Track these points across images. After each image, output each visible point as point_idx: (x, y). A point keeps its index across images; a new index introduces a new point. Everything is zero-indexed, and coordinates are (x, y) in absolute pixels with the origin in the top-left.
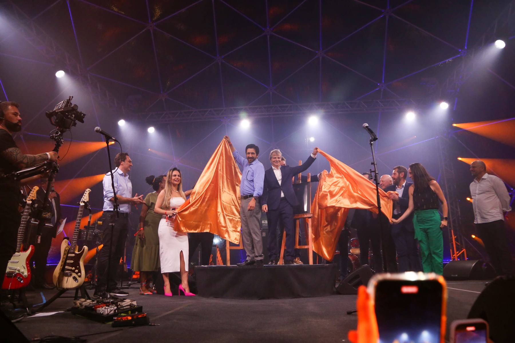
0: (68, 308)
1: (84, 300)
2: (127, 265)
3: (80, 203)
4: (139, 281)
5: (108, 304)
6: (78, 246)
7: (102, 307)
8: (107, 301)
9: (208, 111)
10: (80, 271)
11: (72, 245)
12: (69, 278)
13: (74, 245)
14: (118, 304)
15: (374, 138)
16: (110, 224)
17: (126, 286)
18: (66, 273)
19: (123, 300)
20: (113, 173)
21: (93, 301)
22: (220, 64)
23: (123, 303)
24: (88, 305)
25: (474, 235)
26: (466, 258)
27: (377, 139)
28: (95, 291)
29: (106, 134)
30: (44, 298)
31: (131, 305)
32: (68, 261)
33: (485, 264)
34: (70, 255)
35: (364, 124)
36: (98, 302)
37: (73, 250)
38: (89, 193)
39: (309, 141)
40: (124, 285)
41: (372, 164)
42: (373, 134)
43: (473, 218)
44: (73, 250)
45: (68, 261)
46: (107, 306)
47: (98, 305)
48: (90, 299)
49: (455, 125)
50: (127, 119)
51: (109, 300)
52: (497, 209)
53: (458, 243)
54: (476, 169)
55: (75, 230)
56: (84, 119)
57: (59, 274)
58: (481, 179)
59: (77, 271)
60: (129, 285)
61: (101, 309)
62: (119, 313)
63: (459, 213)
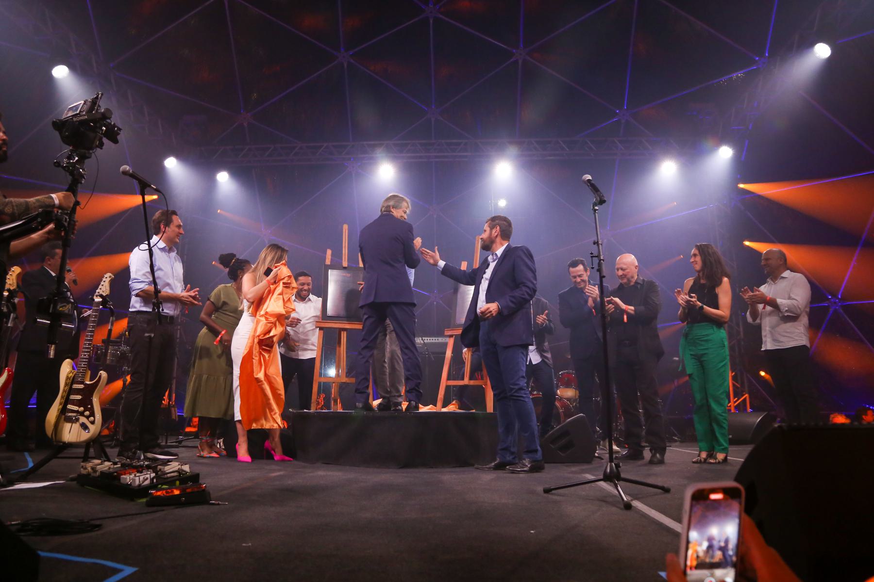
0: (71, 476)
1: (99, 461)
2: (176, 409)
3: (95, 297)
4: (196, 435)
5: (141, 470)
6: (89, 372)
7: (130, 474)
8: (138, 464)
9: (324, 147)
10: (92, 414)
11: (80, 370)
12: (74, 425)
13: (83, 370)
14: (158, 470)
15: (601, 199)
16: (147, 335)
17: (174, 444)
18: (69, 416)
19: (166, 463)
20: (151, 246)
21: (115, 463)
22: (345, 65)
23: (166, 467)
24: (106, 470)
25: (763, 371)
26: (749, 410)
27: (604, 201)
28: (119, 451)
29: (141, 179)
30: (29, 459)
31: (180, 472)
32: (73, 397)
33: (779, 419)
34: (75, 386)
35: (584, 176)
36: (123, 465)
37: (81, 377)
38: (110, 281)
39: (496, 204)
40: (171, 441)
41: (594, 243)
42: (599, 193)
43: (759, 341)
44: (81, 377)
45: (73, 397)
46: (138, 472)
47: (124, 471)
48: (109, 460)
49: (741, 186)
50: (179, 156)
51: (142, 463)
52: (799, 328)
53: (736, 384)
54: (770, 262)
55: (86, 344)
56: (119, 137)
57: (56, 418)
58: (780, 277)
59: (87, 413)
60: (180, 442)
61: (128, 477)
62: (159, 484)
63: (742, 333)
